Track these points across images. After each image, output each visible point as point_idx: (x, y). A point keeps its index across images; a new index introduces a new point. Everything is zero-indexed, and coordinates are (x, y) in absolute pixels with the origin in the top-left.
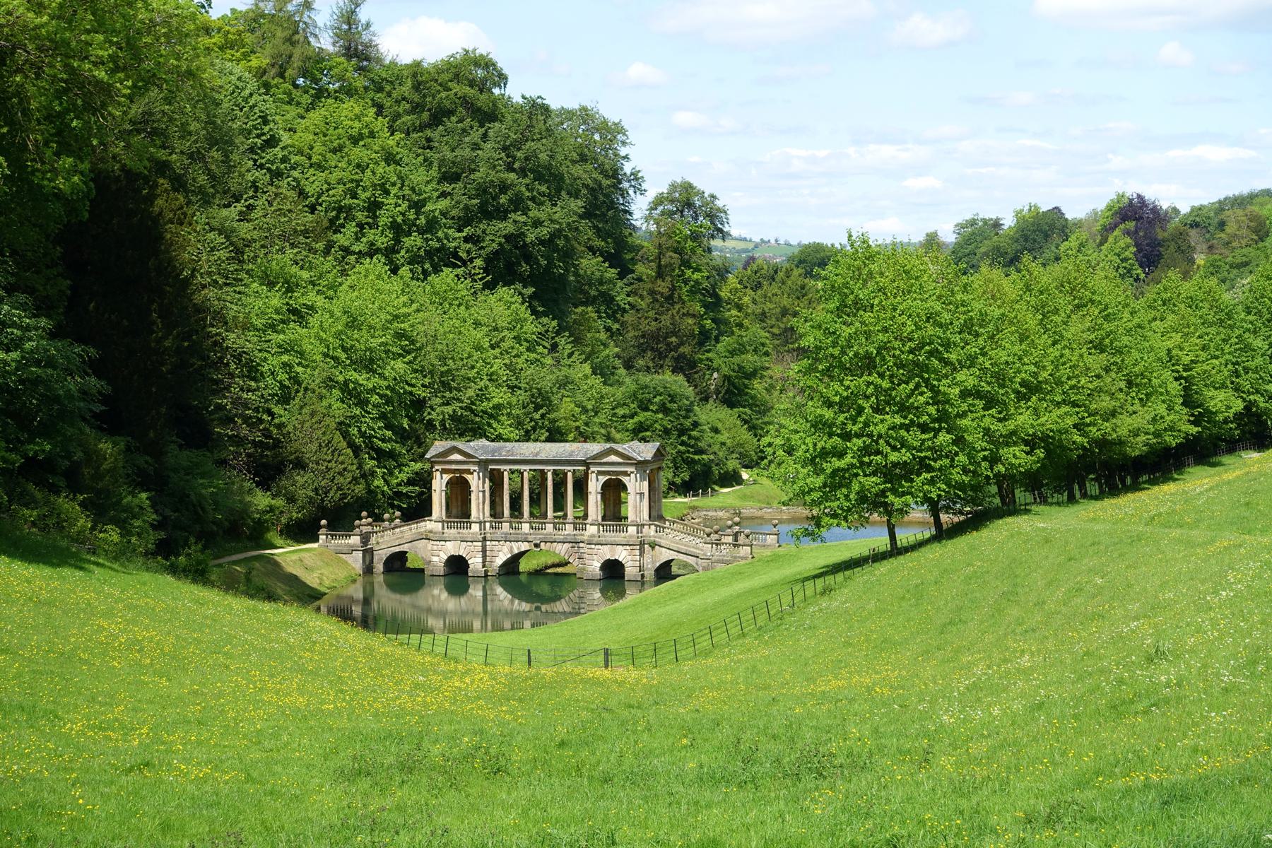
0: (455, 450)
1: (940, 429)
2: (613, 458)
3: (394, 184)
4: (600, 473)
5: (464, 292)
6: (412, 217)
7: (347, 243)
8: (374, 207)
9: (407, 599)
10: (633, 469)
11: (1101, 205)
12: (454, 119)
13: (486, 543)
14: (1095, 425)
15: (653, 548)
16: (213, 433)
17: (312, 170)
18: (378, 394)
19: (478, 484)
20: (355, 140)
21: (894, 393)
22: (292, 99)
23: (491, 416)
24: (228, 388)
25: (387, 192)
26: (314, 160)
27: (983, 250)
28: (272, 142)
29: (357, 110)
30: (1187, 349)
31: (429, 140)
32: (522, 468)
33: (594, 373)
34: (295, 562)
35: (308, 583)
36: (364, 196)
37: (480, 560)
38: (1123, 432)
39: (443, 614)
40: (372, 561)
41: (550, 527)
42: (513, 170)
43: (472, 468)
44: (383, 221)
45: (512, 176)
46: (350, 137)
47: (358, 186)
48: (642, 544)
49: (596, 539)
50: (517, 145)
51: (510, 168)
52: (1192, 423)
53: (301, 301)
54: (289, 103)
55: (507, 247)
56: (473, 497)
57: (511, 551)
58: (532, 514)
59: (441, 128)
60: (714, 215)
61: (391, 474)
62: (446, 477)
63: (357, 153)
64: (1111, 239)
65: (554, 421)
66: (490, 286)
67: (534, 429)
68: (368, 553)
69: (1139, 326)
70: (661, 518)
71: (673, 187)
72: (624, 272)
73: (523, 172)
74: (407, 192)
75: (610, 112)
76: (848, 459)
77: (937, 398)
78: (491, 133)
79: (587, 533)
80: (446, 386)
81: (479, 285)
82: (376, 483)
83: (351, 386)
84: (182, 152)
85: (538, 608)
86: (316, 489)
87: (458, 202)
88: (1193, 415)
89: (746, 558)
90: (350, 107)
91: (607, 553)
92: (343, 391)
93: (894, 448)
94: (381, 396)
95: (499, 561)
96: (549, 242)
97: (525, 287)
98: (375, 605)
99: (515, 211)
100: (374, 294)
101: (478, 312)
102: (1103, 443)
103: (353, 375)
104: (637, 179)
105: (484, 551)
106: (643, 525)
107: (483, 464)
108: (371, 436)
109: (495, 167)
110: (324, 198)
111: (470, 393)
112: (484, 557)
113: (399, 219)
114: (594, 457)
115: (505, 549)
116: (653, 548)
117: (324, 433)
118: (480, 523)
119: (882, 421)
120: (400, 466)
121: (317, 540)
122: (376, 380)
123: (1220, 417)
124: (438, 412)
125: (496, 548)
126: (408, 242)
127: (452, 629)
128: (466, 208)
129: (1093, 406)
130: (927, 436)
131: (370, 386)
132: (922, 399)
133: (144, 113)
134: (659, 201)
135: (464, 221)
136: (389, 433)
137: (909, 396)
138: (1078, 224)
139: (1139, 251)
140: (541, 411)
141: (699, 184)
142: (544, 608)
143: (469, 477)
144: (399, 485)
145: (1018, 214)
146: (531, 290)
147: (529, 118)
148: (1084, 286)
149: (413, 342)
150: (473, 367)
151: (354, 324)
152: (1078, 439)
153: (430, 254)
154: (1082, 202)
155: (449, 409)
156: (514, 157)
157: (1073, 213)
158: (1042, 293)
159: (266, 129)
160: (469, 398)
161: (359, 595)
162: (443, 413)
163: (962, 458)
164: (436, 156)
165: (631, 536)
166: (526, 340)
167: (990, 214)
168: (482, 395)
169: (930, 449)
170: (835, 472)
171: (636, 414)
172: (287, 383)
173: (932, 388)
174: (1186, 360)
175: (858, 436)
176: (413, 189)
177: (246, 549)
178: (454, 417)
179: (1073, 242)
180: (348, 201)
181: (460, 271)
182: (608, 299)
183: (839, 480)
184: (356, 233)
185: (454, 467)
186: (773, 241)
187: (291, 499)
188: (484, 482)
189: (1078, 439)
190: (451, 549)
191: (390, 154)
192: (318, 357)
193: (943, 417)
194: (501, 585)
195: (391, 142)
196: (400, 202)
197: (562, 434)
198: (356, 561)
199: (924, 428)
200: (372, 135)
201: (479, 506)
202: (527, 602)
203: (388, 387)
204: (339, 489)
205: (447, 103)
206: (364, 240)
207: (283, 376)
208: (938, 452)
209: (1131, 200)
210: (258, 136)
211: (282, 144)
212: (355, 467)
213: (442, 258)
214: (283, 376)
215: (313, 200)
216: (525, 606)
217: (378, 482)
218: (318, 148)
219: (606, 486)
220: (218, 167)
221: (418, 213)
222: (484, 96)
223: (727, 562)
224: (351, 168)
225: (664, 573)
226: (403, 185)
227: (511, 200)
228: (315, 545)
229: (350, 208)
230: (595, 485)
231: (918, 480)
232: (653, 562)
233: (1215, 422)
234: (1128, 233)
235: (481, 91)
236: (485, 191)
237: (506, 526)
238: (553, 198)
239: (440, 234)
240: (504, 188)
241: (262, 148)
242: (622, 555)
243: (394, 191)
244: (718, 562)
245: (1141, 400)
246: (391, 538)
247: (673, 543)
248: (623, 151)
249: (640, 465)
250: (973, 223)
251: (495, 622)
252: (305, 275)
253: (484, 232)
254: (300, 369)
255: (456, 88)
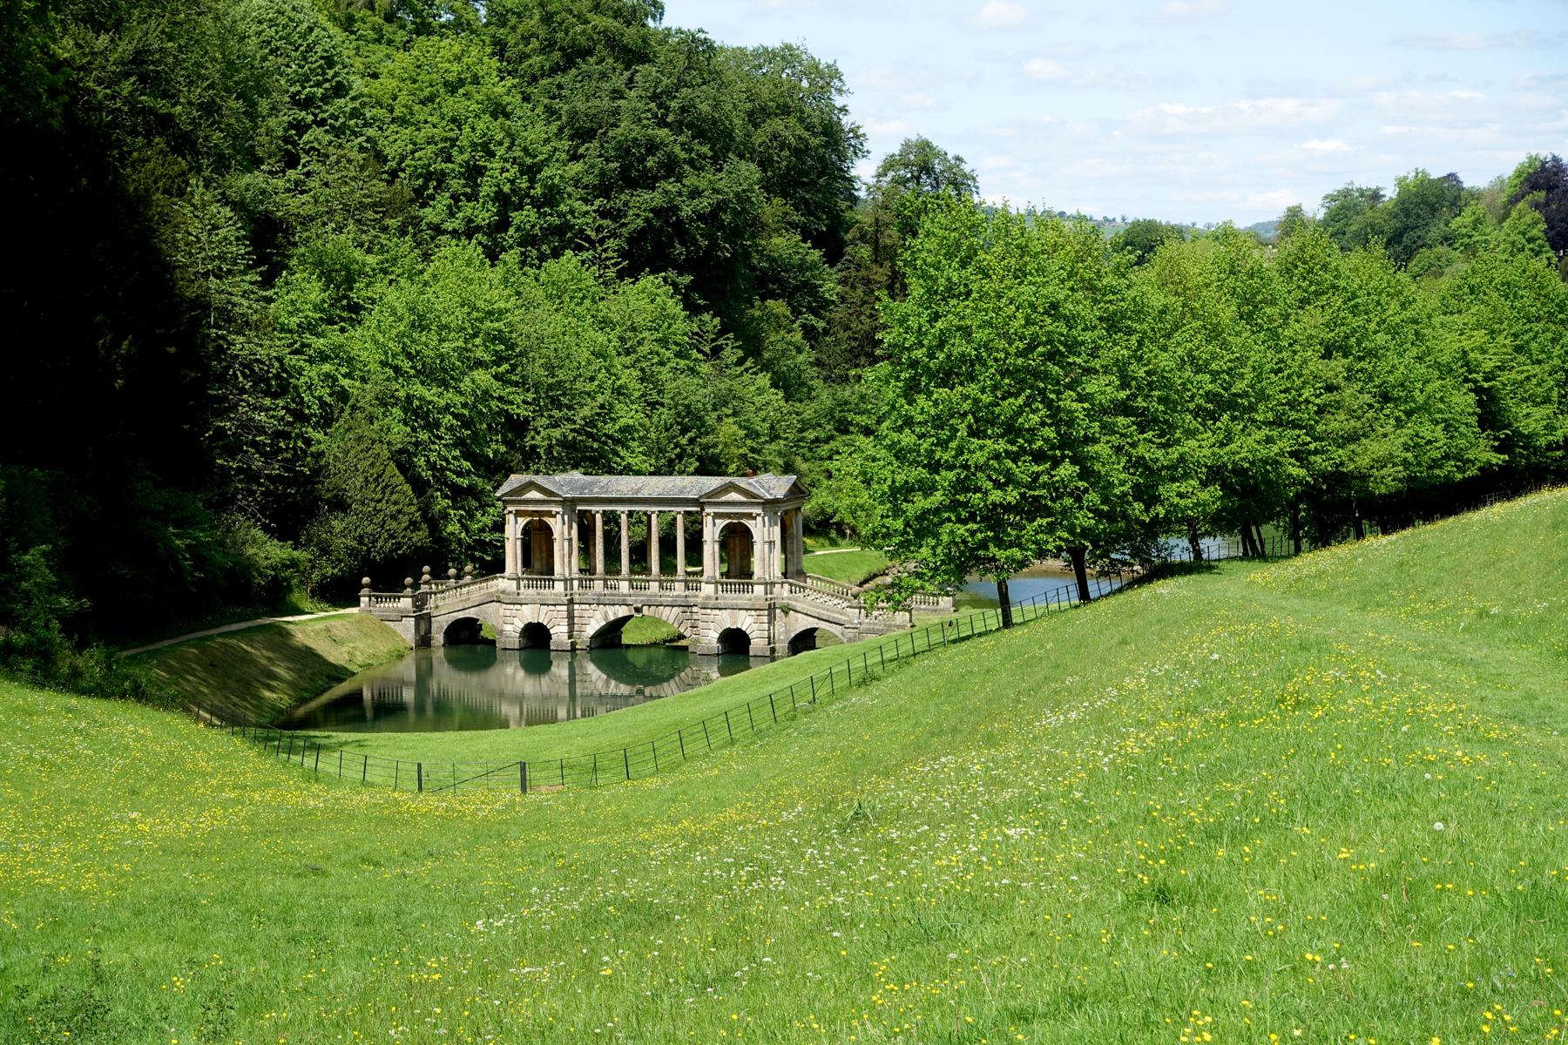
0: (531, 485)
1: (1064, 457)
2: (734, 496)
3: (500, 143)
4: (717, 516)
5: (591, 282)
6: (524, 186)
7: (436, 220)
8: (474, 173)
9: (474, 679)
10: (759, 511)
11: (1508, 171)
12: (592, 60)
13: (573, 605)
14: (1323, 452)
15: (786, 613)
16: (214, 465)
17: (393, 127)
18: (452, 414)
19: (562, 529)
20: (452, 88)
21: (997, 410)
22: (382, 37)
23: (617, 442)
24: (234, 408)
25: (492, 154)
26: (397, 113)
27: (1353, 228)
28: (340, 90)
29: (457, 49)
30: (1492, 351)
31: (560, 87)
32: (649, 509)
33: (774, 385)
34: (318, 633)
35: (331, 659)
36: (459, 159)
37: (565, 629)
38: (1363, 462)
39: (519, 699)
40: (429, 631)
41: (654, 586)
42: (668, 125)
43: (555, 509)
44: (485, 190)
45: (663, 133)
46: (446, 84)
47: (452, 146)
48: (771, 609)
49: (712, 602)
50: (669, 93)
51: (662, 123)
52: (1496, 450)
53: (363, 293)
54: (378, 41)
55: (656, 223)
56: (756, 547)
57: (606, 617)
58: (632, 572)
59: (574, 71)
60: (960, 182)
61: (471, 516)
62: (522, 521)
63: (453, 104)
64: (1514, 214)
65: (706, 447)
66: (631, 272)
67: (680, 457)
68: (423, 620)
69: (1415, 322)
70: (801, 574)
71: (907, 146)
72: (833, 257)
73: (677, 128)
74: (518, 153)
75: (821, 51)
76: (938, 497)
77: (1056, 415)
78: (638, 77)
79: (702, 594)
80: (555, 402)
81: (611, 273)
82: (450, 529)
83: (416, 403)
84: (190, 103)
85: (640, 692)
86: (361, 537)
87: (592, 167)
88: (1496, 438)
89: (903, 627)
90: (450, 45)
91: (726, 620)
92: (405, 410)
93: (998, 485)
94: (456, 416)
95: (592, 628)
96: (710, 218)
97: (680, 274)
98: (433, 686)
99: (665, 178)
100: (459, 283)
101: (612, 308)
102: (1338, 478)
103: (418, 389)
104: (857, 137)
105: (571, 617)
106: (773, 584)
107: (569, 504)
108: (443, 469)
109: (640, 120)
110: (407, 162)
111: (586, 411)
112: (571, 624)
113: (506, 188)
114: (710, 495)
115: (598, 615)
116: (786, 613)
117: (372, 464)
118: (565, 580)
119: (981, 448)
120: (483, 506)
121: (357, 604)
122: (450, 396)
123: (1542, 442)
124: (542, 436)
125: (586, 614)
126: (517, 217)
127: (532, 720)
128: (603, 173)
129: (1320, 428)
130: (1041, 468)
131: (443, 403)
132: (1035, 418)
133: (137, 53)
134: (889, 164)
135: (604, 189)
136: (467, 465)
137: (1019, 413)
138: (1475, 195)
139: (1551, 228)
140: (689, 435)
141: (939, 143)
142: (647, 691)
143: (749, 523)
144: (482, 530)
145: (1401, 182)
146: (687, 279)
147: (688, 58)
148: (1325, 267)
149: (512, 347)
150: (592, 379)
151: (420, 324)
152: (1297, 471)
153: (551, 231)
154: (1486, 162)
155: (557, 433)
156: (667, 108)
157: (1469, 181)
158: (1252, 276)
159: (331, 73)
160: (584, 418)
161: (411, 675)
162: (549, 438)
163: (1093, 497)
164: (566, 107)
165: (757, 598)
166: (676, 343)
167: (1366, 182)
168: (606, 412)
169: (1044, 486)
170: (923, 516)
171: (832, 438)
172: (328, 399)
173: (1049, 404)
174: (1488, 366)
175: (951, 468)
176: (525, 150)
177: (258, 616)
178: (563, 443)
179: (1466, 218)
180: (440, 166)
181: (585, 255)
182: (811, 289)
183: (924, 527)
184: (449, 207)
185: (531, 508)
186: (1119, 220)
187: (325, 550)
188: (570, 528)
189: (1297, 471)
190: (528, 614)
191: (498, 104)
192: (373, 367)
193: (1065, 442)
194: (593, 660)
195: (499, 90)
196: (508, 166)
197: (720, 465)
198: (406, 630)
199: (1039, 457)
200: (476, 80)
201: (565, 559)
202: (627, 683)
203: (465, 405)
204: (392, 536)
205: (582, 40)
206: (460, 215)
207: (324, 392)
208: (1058, 490)
209: (1544, 163)
210: (318, 84)
211: (352, 93)
212: (413, 509)
213: (562, 237)
214: (324, 392)
215: (394, 164)
216: (624, 689)
217: (453, 527)
218: (403, 98)
219: (526, 531)
220: (238, 120)
221: (532, 181)
222: (632, 30)
223: (880, 633)
224: (444, 123)
225: (804, 641)
226: (512, 144)
227: (661, 164)
228: (355, 610)
229: (443, 174)
230: (711, 532)
231: (1030, 528)
232: (787, 632)
233: (1535, 448)
234: (1537, 206)
235: (629, 24)
236: (628, 151)
237: (598, 585)
238: (717, 160)
239: (563, 208)
240: (652, 147)
241: (325, 99)
242: (745, 622)
243: (501, 151)
244: (868, 632)
245: (1398, 419)
246: (452, 601)
247: (811, 606)
248: (839, 101)
249: (769, 505)
250: (1346, 193)
251: (581, 704)
252: (371, 260)
253: (626, 204)
254: (346, 382)
255: (597, 20)
